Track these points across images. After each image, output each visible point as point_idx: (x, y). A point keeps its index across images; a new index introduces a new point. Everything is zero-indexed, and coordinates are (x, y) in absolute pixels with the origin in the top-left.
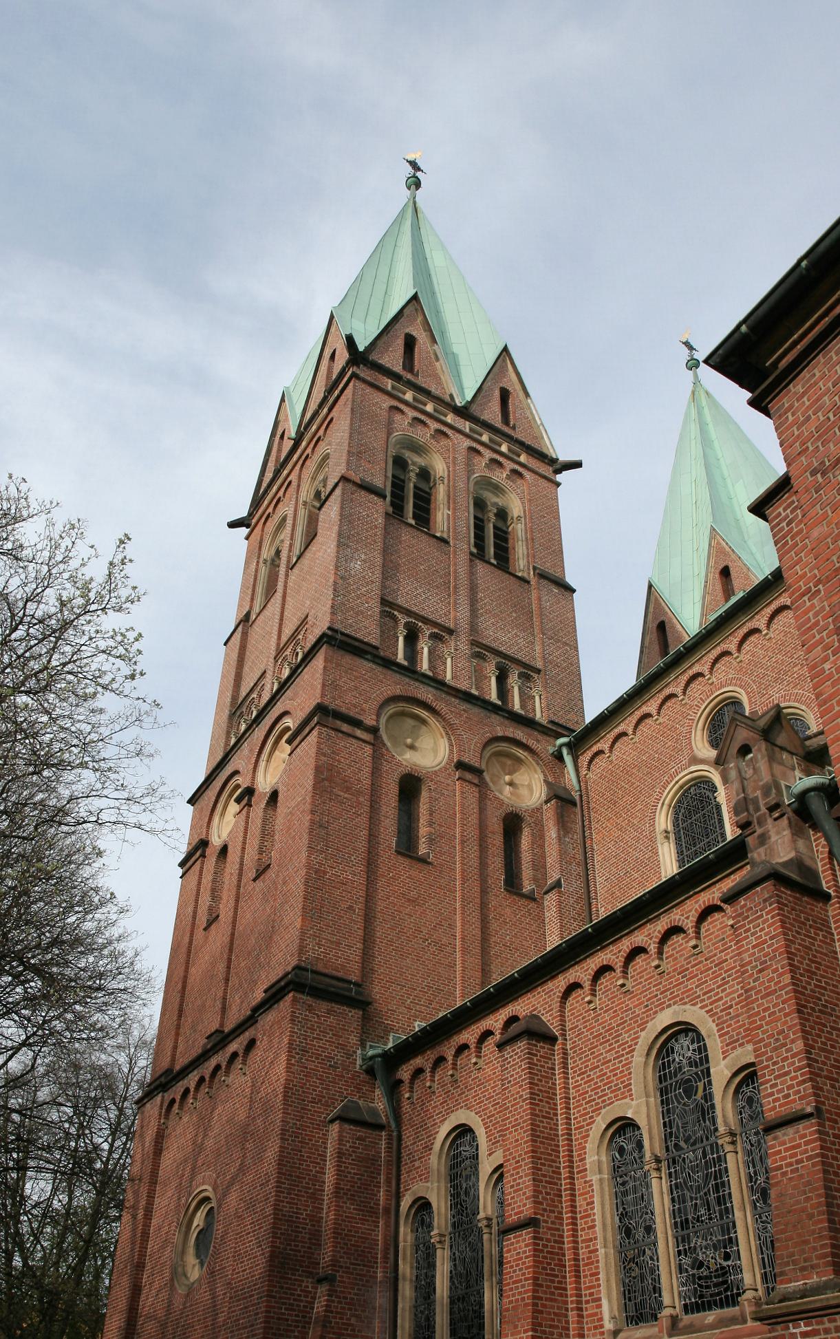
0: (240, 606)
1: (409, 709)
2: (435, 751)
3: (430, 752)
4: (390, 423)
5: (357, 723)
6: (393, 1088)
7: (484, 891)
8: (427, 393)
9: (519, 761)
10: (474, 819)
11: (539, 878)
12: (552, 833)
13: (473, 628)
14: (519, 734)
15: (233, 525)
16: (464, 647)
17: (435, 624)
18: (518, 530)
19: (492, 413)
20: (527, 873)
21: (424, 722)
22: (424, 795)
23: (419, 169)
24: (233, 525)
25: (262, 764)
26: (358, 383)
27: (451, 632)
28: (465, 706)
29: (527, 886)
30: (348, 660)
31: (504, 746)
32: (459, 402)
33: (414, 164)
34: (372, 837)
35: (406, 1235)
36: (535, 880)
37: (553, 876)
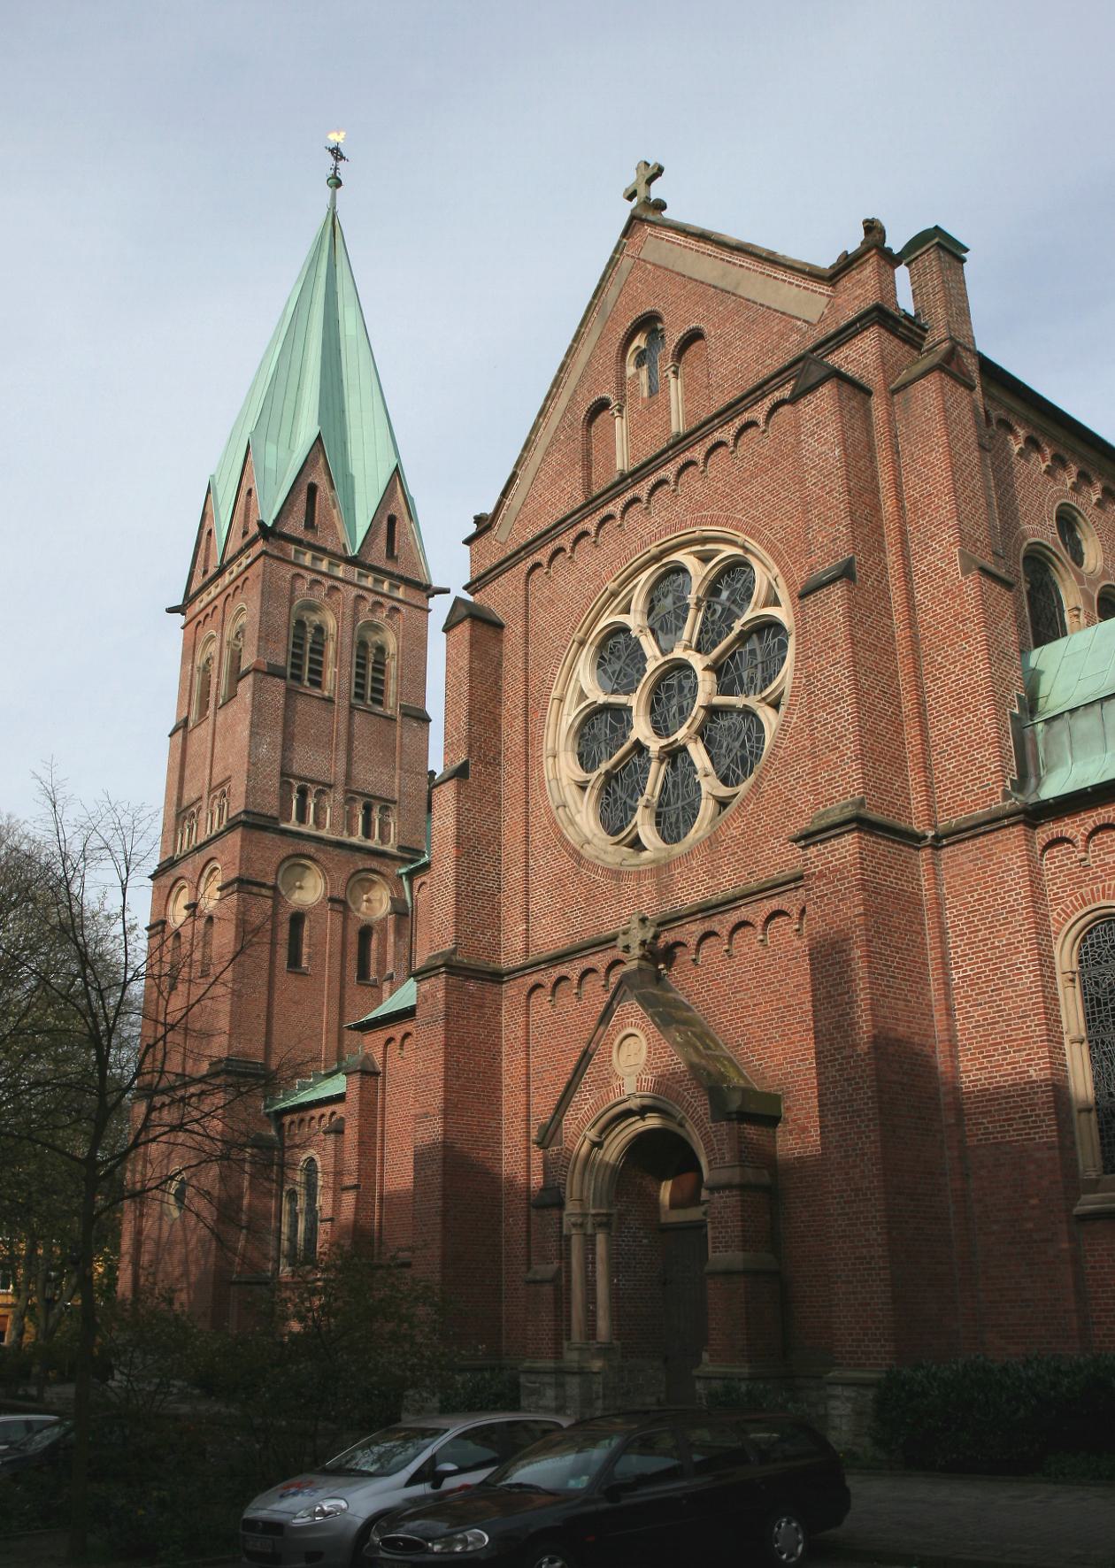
0: (178, 715)
1: (295, 863)
2: (315, 888)
3: (311, 891)
4: (293, 590)
5: (263, 885)
6: (280, 1128)
7: (342, 987)
8: (323, 550)
9: (374, 882)
10: (338, 938)
11: (380, 972)
12: (391, 938)
13: (348, 776)
14: (374, 864)
15: (171, 610)
16: (340, 797)
17: (319, 783)
18: (392, 665)
19: (378, 556)
20: (373, 966)
21: (308, 868)
22: (306, 923)
23: (342, 158)
24: (171, 610)
25: (203, 880)
26: (269, 561)
27: (330, 786)
28: (338, 851)
29: (373, 976)
30: (257, 835)
31: (363, 875)
32: (352, 552)
33: (336, 153)
34: (272, 962)
35: (286, 1206)
36: (378, 972)
37: (390, 970)
